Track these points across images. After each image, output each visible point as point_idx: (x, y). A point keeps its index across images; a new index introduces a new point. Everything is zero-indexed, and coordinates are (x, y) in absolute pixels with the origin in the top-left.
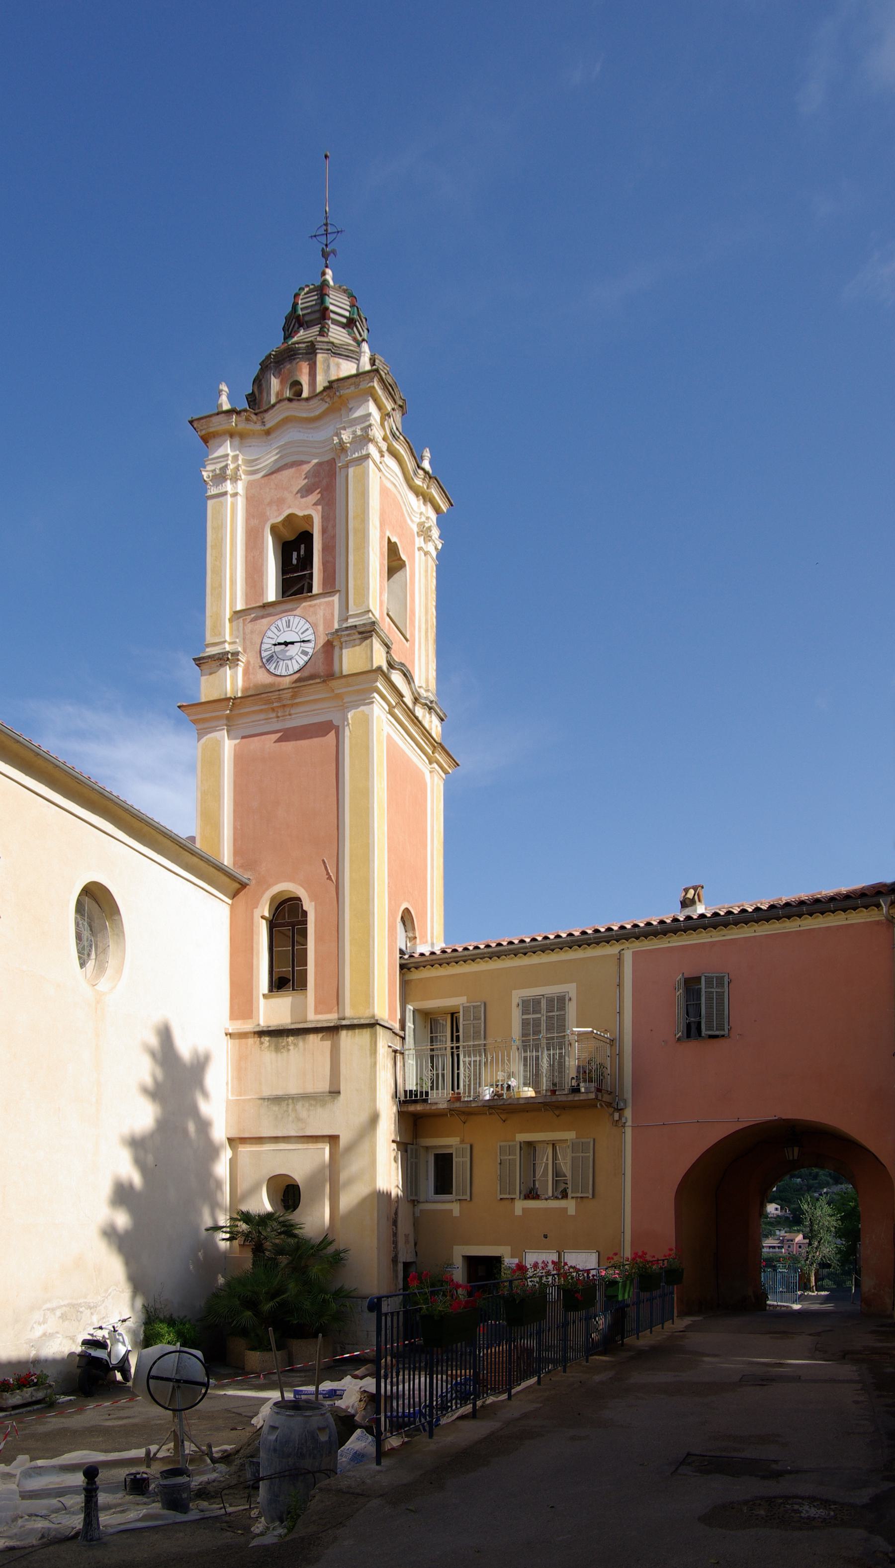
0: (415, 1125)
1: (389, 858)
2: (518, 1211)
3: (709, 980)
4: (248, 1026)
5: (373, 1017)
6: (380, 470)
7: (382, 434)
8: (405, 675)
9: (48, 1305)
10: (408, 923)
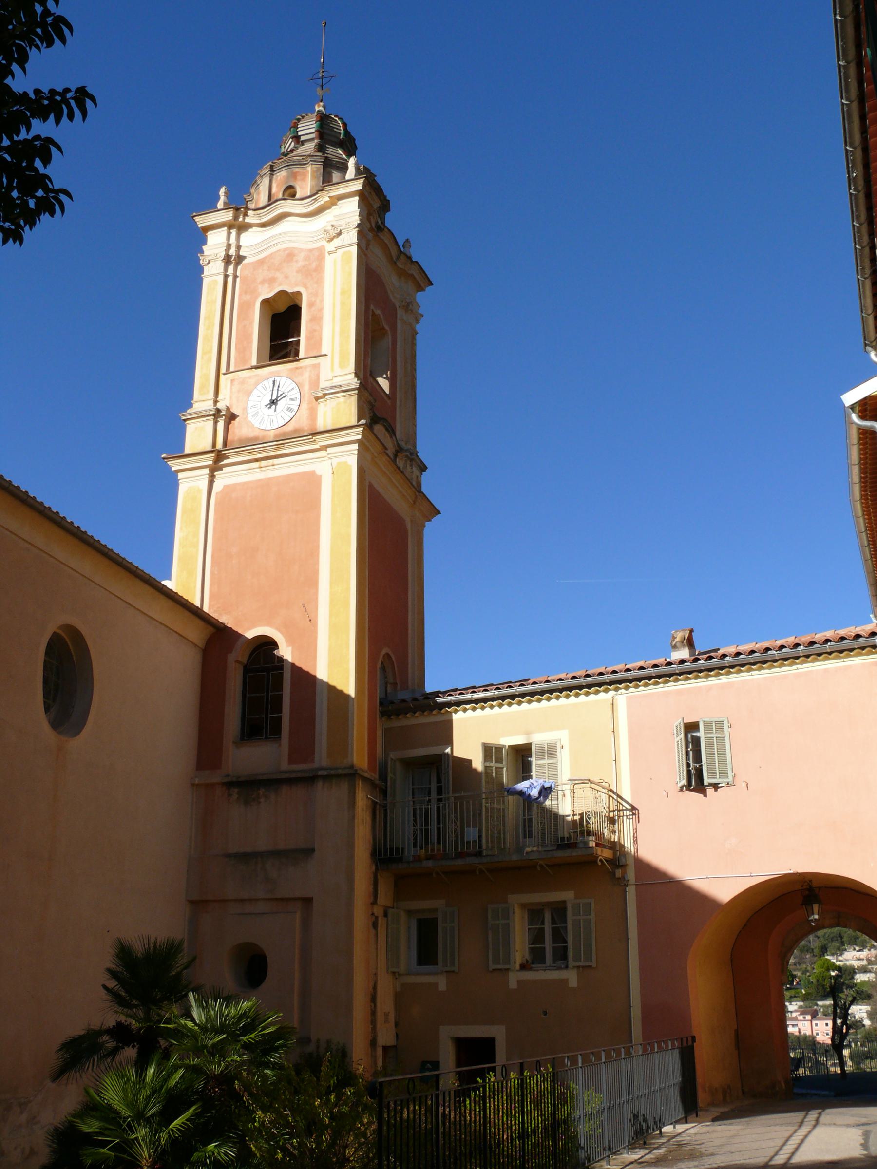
2: (513, 984)
3: (708, 725)
4: (216, 778)
5: (352, 766)
7: (369, 226)
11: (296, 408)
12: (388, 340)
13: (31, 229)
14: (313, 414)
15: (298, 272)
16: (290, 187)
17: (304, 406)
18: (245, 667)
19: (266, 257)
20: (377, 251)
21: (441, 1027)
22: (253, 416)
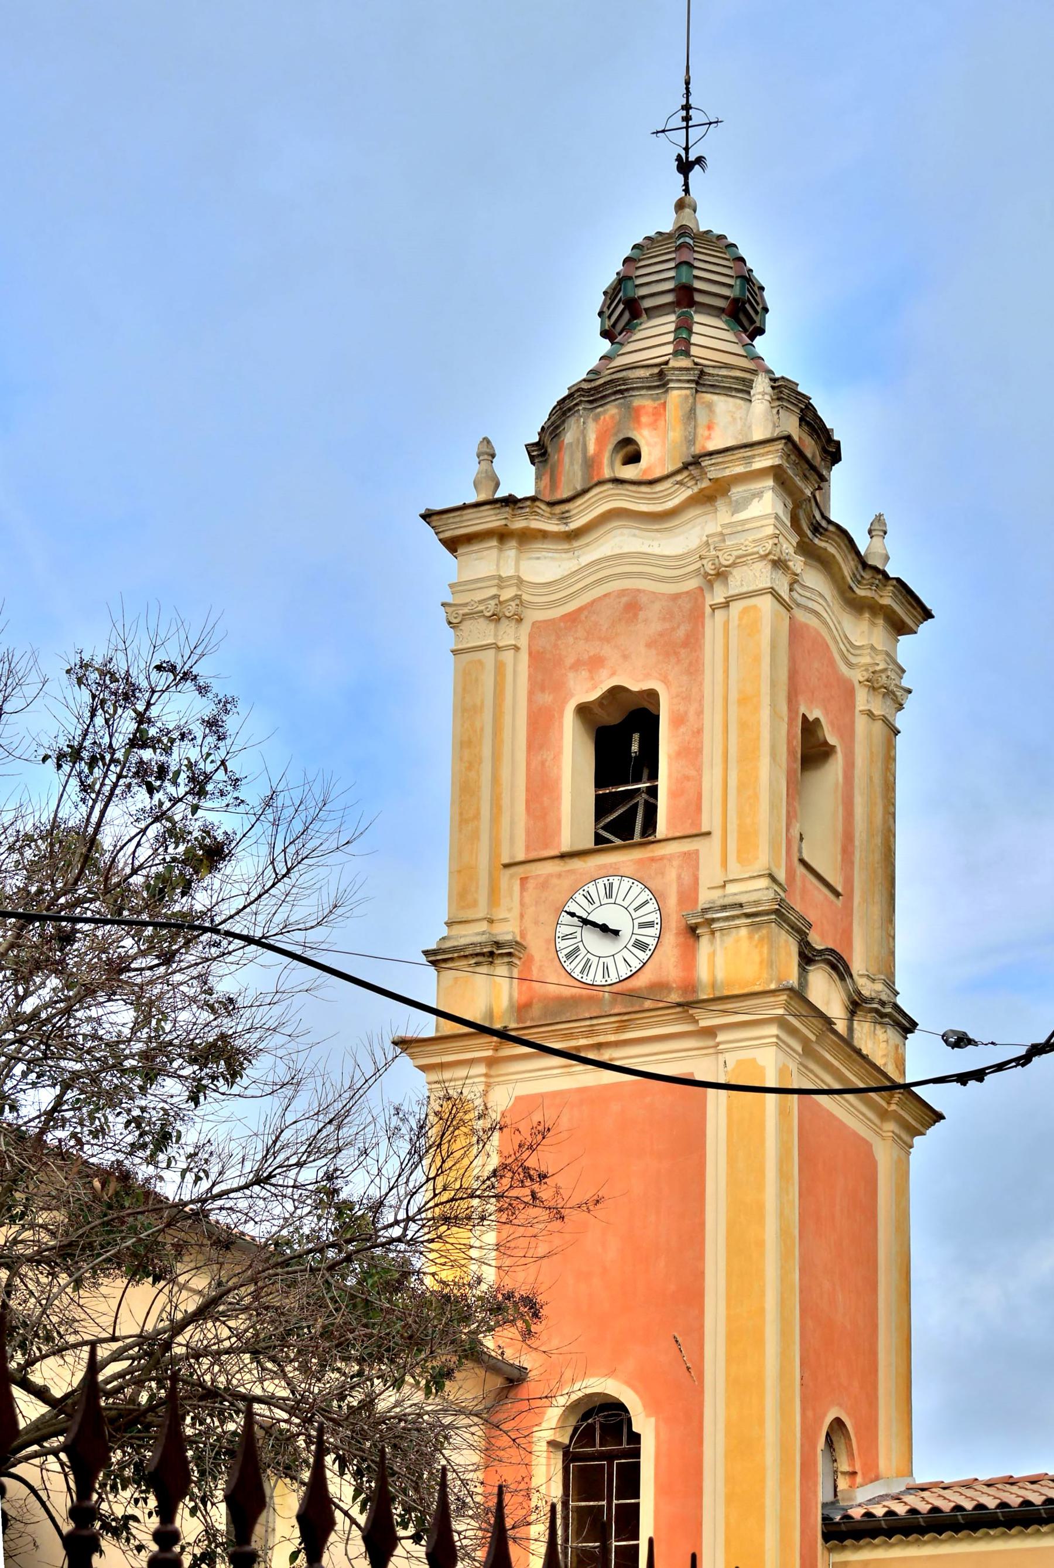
8: (834, 967)
12: (834, 770)
16: (628, 441)
19: (580, 610)
22: (568, 956)
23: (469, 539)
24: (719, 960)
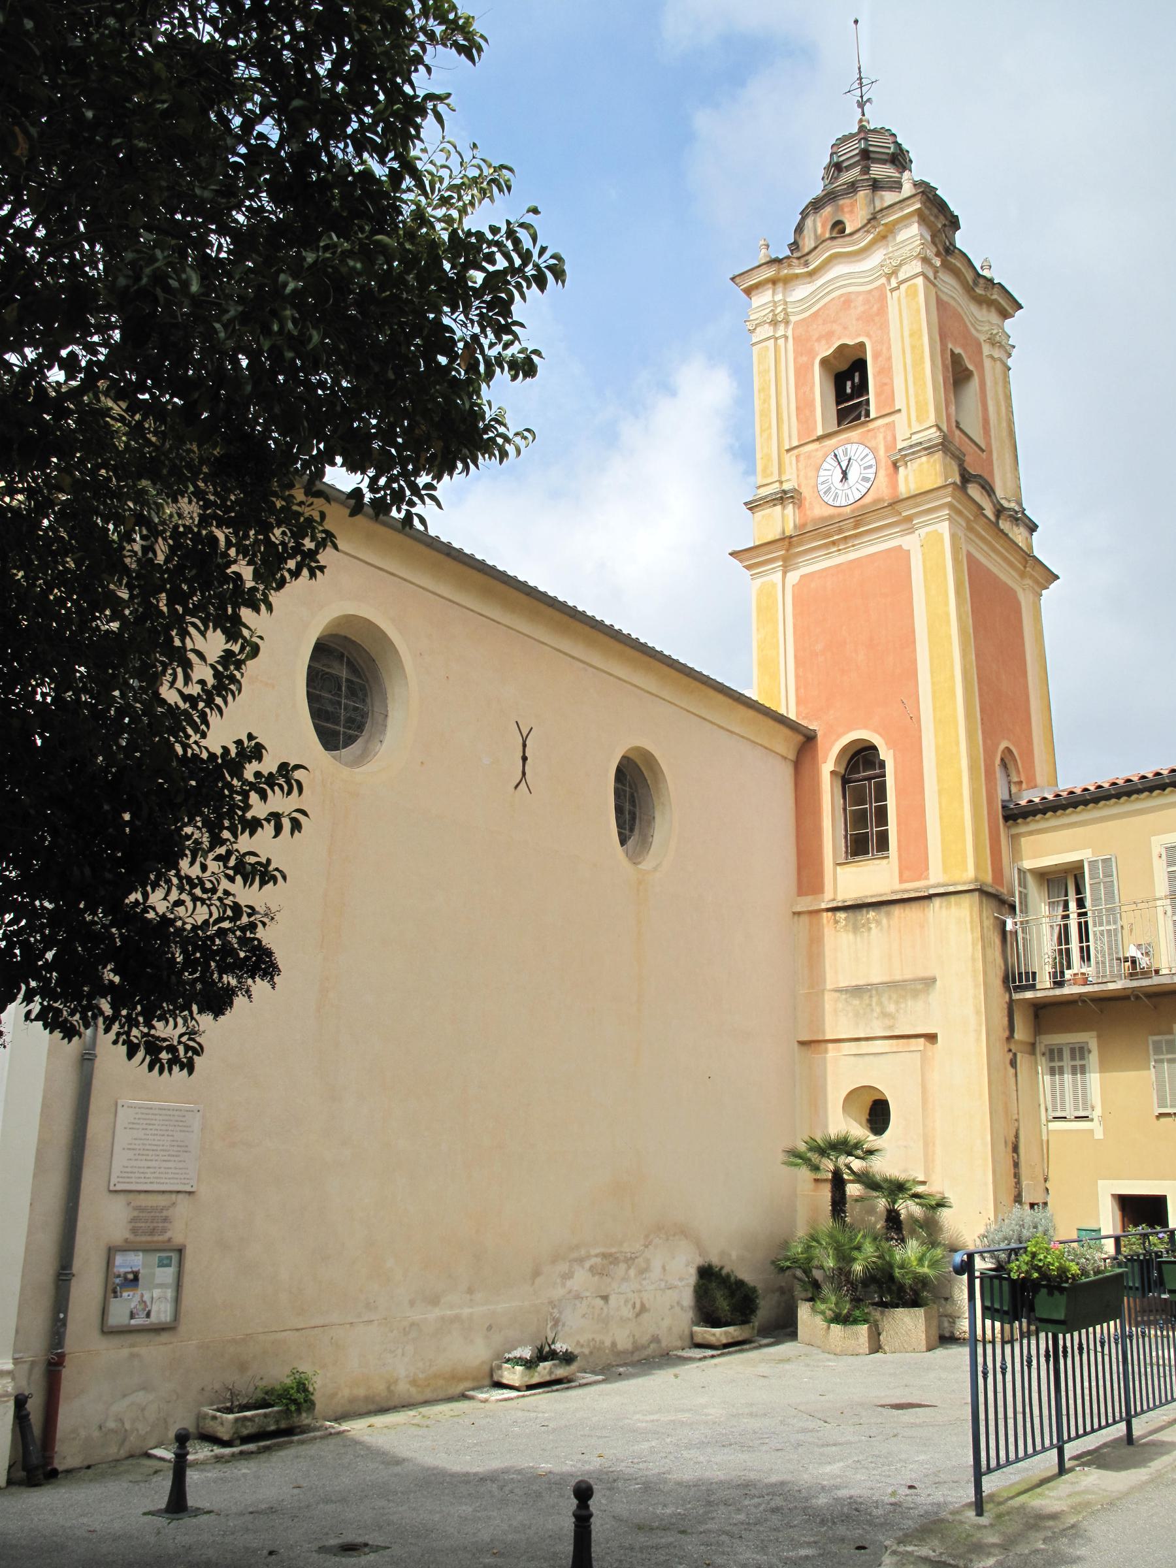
0: (1036, 1016)
1: (980, 689)
6: (935, 285)
7: (934, 250)
8: (983, 488)
9: (575, 1255)
10: (1011, 766)
11: (872, 476)
12: (975, 382)
13: (251, 835)
14: (894, 484)
15: (858, 319)
17: (882, 473)
18: (843, 778)
19: (819, 309)
20: (949, 284)
21: (1100, 1182)
23: (757, 286)
24: (911, 478)
